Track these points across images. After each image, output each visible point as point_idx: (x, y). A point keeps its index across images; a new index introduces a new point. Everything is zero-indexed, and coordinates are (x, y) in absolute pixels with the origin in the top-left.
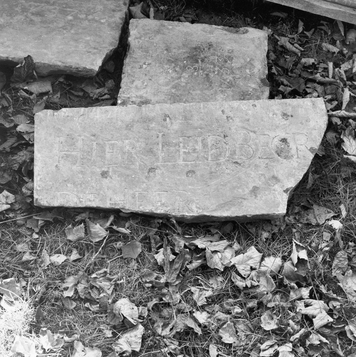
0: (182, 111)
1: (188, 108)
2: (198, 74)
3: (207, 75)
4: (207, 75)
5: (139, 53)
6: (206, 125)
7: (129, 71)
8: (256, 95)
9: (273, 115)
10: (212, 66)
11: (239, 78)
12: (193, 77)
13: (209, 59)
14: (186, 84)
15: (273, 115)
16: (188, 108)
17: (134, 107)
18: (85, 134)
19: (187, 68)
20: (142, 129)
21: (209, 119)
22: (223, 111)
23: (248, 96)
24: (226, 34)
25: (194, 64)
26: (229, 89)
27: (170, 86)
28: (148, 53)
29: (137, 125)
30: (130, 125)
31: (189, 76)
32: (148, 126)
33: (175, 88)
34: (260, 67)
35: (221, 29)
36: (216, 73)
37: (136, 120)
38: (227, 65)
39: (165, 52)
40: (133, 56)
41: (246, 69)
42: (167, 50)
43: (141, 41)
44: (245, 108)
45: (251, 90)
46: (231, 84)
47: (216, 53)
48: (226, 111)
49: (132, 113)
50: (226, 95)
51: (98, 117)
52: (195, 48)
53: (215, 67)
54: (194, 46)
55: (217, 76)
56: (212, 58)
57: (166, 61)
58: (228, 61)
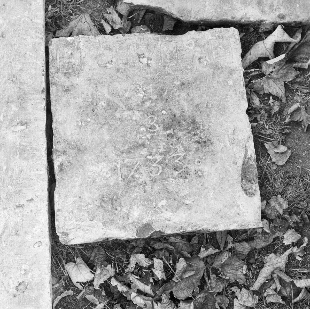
0: (34, 146)
1: (37, 154)
2: (142, 133)
3: (143, 145)
4: (143, 145)
5: (167, 49)
6: (11, 177)
7: (128, 42)
8: (116, 218)
9: (25, 270)
10: (162, 150)
11: (145, 191)
12: (136, 127)
13: (176, 145)
14: (119, 119)
15: (25, 270)
16: (37, 154)
17: (42, 84)
18: (5, 25)
19: (151, 116)
20: (8, 94)
21: (21, 182)
22: (32, 200)
23: (110, 207)
24: (235, 163)
25: (162, 125)
26: (120, 179)
27: (111, 98)
28: (170, 59)
29: (15, 88)
30: (14, 79)
31: (136, 120)
32: (13, 102)
33: (108, 105)
34: (176, 220)
35: (246, 155)
36: (148, 157)
37: (22, 87)
38: (169, 172)
39: (178, 83)
40: (160, 42)
41: (167, 199)
42: (183, 84)
43: (192, 48)
44: (36, 231)
45: (125, 210)
46: (130, 181)
47: (192, 153)
48: (32, 204)
49: (32, 82)
50: (108, 176)
51: (29, 40)
52: (194, 122)
53: (162, 154)
54: (198, 120)
55: (143, 159)
56: (180, 148)
57: (159, 86)
58: (177, 173)
